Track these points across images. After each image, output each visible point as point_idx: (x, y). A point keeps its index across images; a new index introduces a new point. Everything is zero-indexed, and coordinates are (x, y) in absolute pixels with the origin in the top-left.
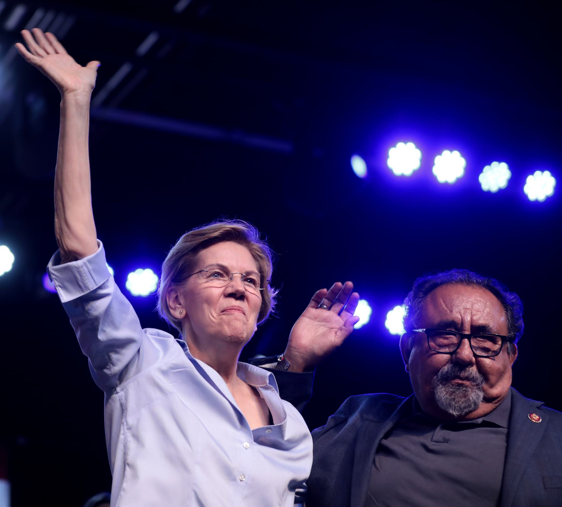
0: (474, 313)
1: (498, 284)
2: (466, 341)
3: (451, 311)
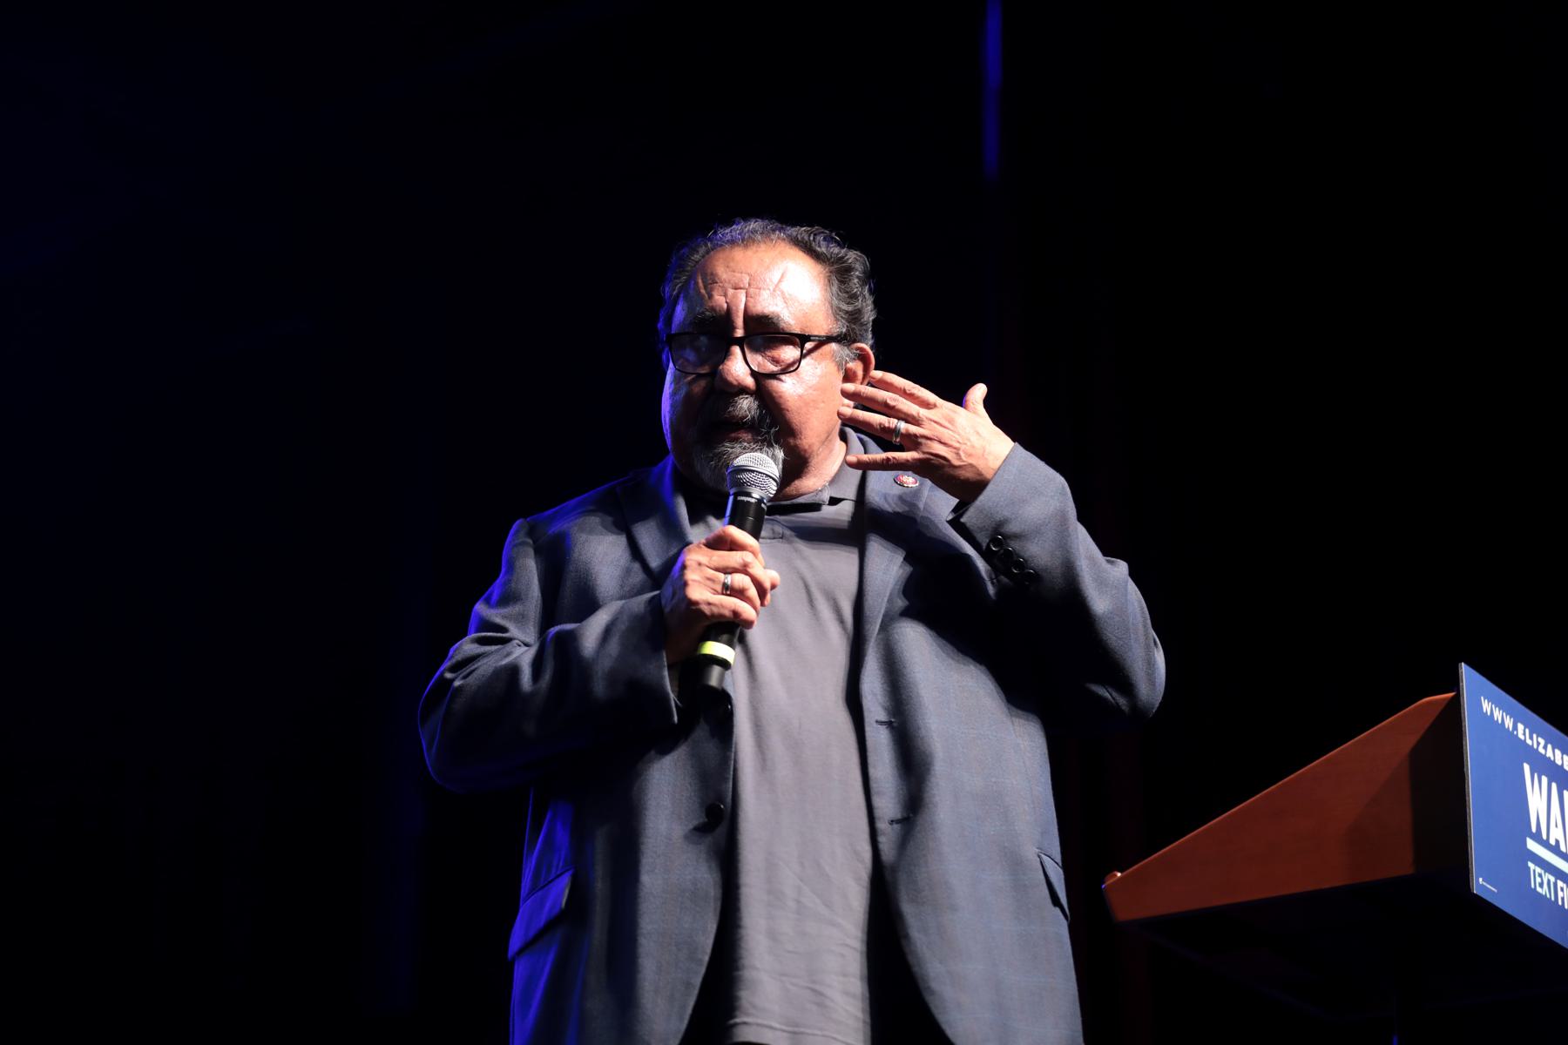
0: (752, 291)
2: (736, 350)
3: (711, 297)
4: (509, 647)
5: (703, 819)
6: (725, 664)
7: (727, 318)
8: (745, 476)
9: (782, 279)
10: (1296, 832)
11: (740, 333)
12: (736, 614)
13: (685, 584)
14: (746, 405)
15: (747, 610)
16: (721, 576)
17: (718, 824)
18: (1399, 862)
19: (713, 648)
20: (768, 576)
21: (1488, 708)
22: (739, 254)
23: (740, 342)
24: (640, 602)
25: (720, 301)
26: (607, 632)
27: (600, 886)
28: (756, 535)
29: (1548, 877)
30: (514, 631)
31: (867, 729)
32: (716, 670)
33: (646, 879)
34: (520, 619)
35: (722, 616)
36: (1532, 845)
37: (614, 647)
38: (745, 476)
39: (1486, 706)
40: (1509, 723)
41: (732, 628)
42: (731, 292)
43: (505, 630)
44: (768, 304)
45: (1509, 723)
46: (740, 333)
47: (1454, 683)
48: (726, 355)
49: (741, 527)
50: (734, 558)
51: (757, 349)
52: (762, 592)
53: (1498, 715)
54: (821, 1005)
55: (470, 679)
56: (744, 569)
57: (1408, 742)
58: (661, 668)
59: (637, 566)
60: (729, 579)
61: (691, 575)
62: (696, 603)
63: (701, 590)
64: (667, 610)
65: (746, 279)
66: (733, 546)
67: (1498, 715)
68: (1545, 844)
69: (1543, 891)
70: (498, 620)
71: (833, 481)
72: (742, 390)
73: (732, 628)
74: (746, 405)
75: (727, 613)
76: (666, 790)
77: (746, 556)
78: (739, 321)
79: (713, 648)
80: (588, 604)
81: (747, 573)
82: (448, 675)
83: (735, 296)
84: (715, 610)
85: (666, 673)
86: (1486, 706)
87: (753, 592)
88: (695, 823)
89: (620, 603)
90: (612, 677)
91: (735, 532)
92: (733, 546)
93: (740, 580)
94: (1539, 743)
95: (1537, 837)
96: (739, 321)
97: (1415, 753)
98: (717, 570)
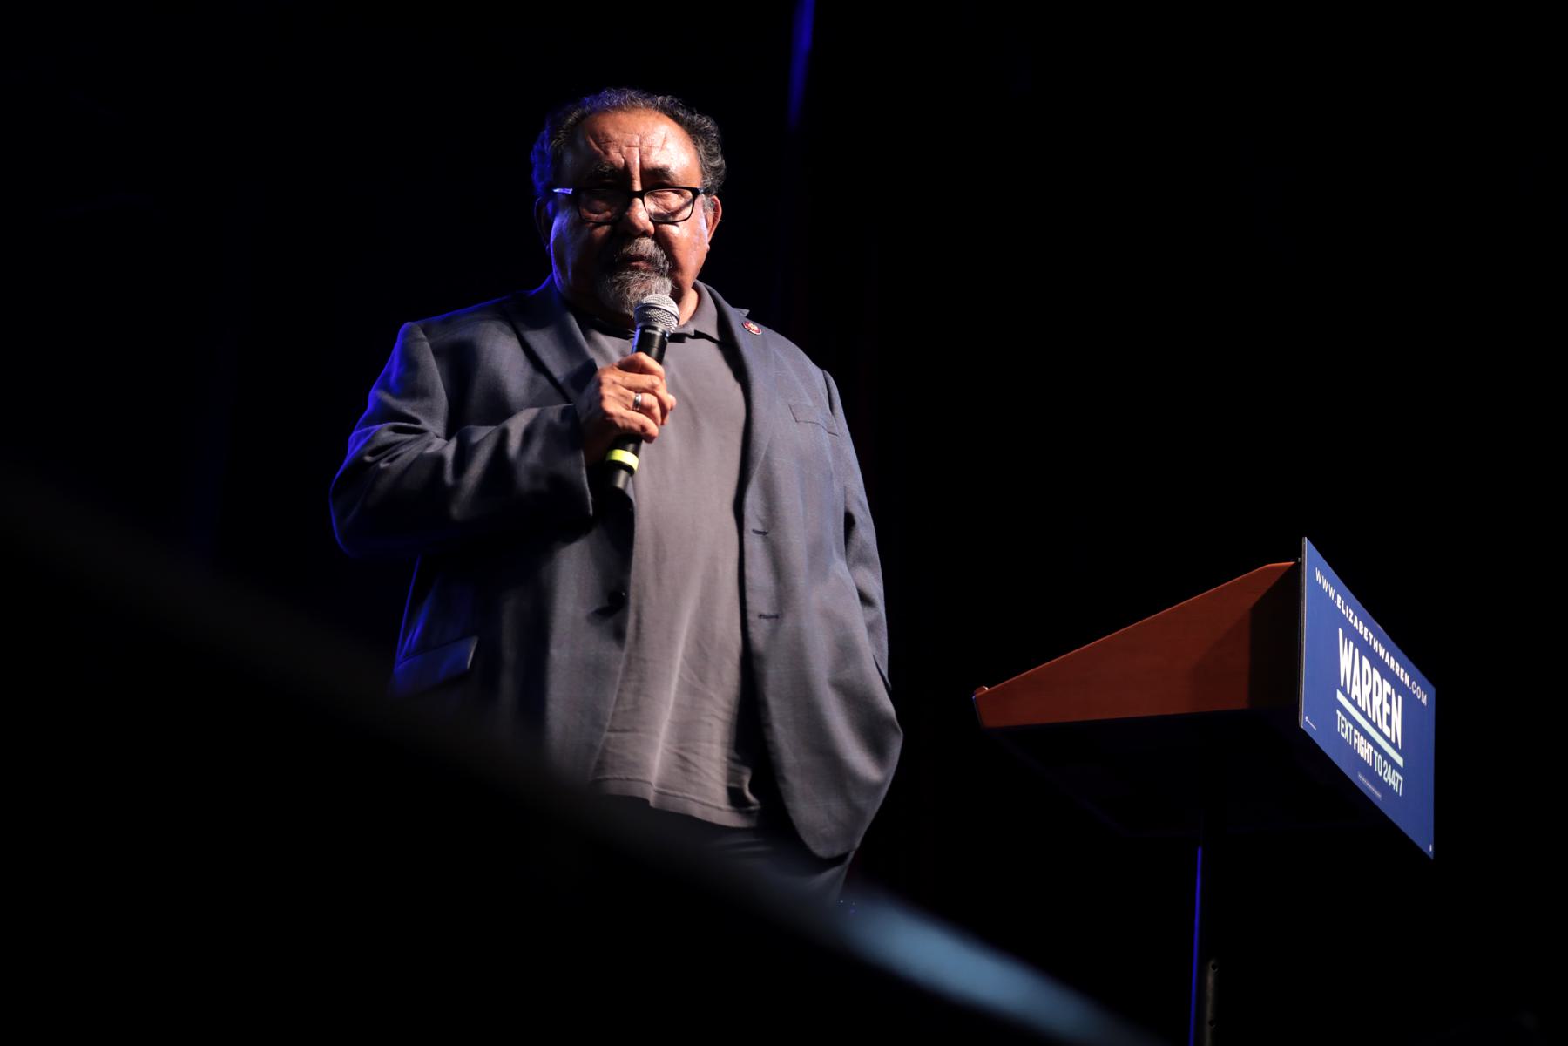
0: (644, 148)
1: (688, 102)
2: (638, 200)
3: (607, 153)
4: (427, 438)
5: (606, 604)
6: (629, 470)
7: (626, 171)
8: (653, 313)
9: (661, 142)
10: (1141, 669)
11: (638, 187)
12: (643, 428)
13: (601, 398)
14: (647, 245)
15: (653, 428)
16: (633, 394)
17: (613, 606)
18: (1235, 697)
19: (622, 456)
20: (670, 399)
21: (1320, 579)
22: (623, 117)
23: (641, 195)
24: (554, 412)
25: (617, 157)
26: (528, 435)
27: (509, 654)
28: (660, 360)
29: (1349, 725)
30: (425, 424)
31: (746, 536)
32: (623, 474)
33: (555, 652)
34: (430, 412)
35: (631, 429)
36: (1340, 697)
37: (536, 447)
38: (653, 313)
39: (1319, 576)
40: (1332, 593)
41: (634, 438)
42: (625, 149)
43: (417, 421)
44: (658, 159)
45: (1332, 593)
46: (638, 187)
47: (1298, 552)
48: (629, 204)
49: (648, 354)
50: (644, 380)
51: (655, 196)
52: (664, 412)
53: (1325, 585)
54: (685, 770)
55: (396, 463)
56: (651, 390)
57: (1249, 601)
58: (580, 466)
59: (543, 380)
60: (639, 398)
61: (607, 391)
62: (611, 415)
63: (614, 405)
64: (582, 420)
65: (637, 139)
66: (644, 370)
67: (1325, 585)
68: (1348, 697)
69: (1345, 735)
70: (408, 411)
71: (692, 318)
72: (645, 234)
73: (634, 438)
74: (647, 245)
75: (637, 427)
76: (573, 573)
77: (656, 380)
78: (637, 174)
79: (622, 456)
80: (500, 409)
81: (654, 393)
82: (368, 459)
83: (629, 152)
84: (627, 424)
85: (584, 472)
86: (1319, 576)
87: (657, 411)
88: (597, 606)
89: (534, 411)
90: (535, 474)
91: (649, 361)
92: (644, 370)
93: (648, 399)
94: (1348, 613)
95: (1343, 690)
96: (637, 174)
97: (1256, 609)
98: (629, 388)
